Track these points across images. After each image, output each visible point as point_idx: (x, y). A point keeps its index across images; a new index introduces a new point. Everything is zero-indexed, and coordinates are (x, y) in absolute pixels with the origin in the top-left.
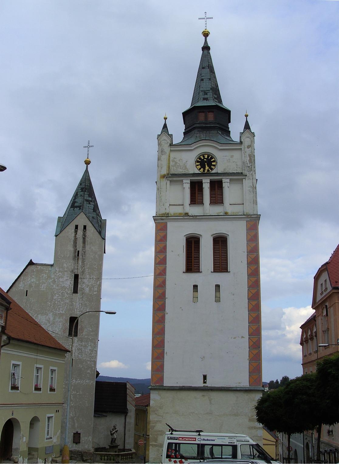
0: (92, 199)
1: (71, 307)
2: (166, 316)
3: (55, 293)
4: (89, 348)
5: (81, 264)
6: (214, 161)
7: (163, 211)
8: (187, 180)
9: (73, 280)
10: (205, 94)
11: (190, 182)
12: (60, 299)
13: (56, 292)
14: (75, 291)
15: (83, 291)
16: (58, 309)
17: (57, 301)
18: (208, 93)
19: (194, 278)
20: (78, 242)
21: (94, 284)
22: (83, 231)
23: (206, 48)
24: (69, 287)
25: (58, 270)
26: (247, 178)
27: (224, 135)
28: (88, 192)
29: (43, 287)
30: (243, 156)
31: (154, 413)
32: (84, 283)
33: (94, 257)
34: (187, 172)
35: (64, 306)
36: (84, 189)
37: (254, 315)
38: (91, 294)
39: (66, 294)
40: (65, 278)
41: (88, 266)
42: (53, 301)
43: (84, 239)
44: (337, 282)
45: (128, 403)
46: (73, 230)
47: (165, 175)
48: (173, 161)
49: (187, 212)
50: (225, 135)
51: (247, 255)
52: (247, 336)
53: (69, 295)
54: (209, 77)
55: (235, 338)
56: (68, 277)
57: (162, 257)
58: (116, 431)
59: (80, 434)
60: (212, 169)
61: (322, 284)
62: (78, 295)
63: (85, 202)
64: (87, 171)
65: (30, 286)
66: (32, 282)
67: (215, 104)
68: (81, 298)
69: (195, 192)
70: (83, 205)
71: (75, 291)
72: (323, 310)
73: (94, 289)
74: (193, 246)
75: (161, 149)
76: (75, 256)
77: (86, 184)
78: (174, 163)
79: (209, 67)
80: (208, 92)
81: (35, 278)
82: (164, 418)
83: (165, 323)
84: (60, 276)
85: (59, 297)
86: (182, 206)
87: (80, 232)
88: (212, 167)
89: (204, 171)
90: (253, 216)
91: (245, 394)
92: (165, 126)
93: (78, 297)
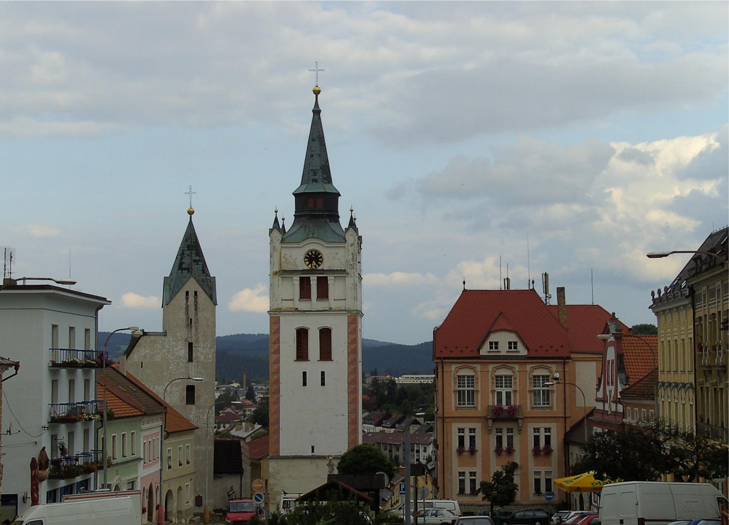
6: (321, 261)
12: (176, 368)
14: (190, 359)
19: (303, 366)
23: (317, 112)
26: (349, 276)
28: (195, 250)
29: (158, 358)
30: (347, 254)
32: (198, 351)
34: (296, 269)
43: (196, 306)
46: (184, 297)
48: (284, 257)
49: (297, 307)
54: (319, 153)
55: (337, 416)
58: (233, 493)
59: (201, 497)
60: (319, 265)
62: (194, 363)
63: (194, 263)
64: (191, 223)
65: (145, 357)
76: (188, 324)
78: (285, 260)
79: (319, 138)
80: (317, 171)
86: (292, 301)
88: (319, 263)
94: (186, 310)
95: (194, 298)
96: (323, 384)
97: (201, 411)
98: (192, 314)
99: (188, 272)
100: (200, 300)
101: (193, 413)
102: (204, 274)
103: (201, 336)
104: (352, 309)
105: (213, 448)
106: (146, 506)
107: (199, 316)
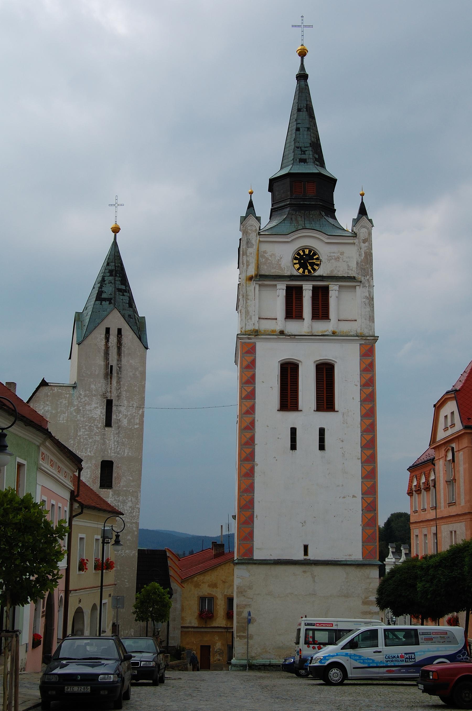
0: (126, 287)
1: (103, 447)
2: (256, 468)
3: (80, 427)
4: (129, 504)
5: (115, 385)
7: (250, 327)
8: (282, 285)
9: (105, 408)
10: (303, 153)
11: (285, 288)
12: (87, 434)
13: (81, 426)
14: (108, 423)
15: (120, 424)
16: (84, 450)
17: (83, 438)
18: (306, 151)
20: (110, 353)
21: (134, 414)
22: (118, 336)
24: (100, 418)
25: (83, 394)
27: (329, 217)
28: (119, 277)
31: (242, 595)
32: (120, 412)
33: (133, 374)
35: (94, 446)
36: (114, 272)
37: (369, 468)
38: (131, 428)
39: (96, 428)
40: (94, 405)
41: (126, 388)
42: (77, 439)
44: (470, 419)
45: (171, 579)
46: (103, 336)
47: (253, 276)
50: (329, 216)
51: (360, 389)
52: (359, 496)
53: (99, 430)
55: (344, 497)
56: (97, 404)
57: (249, 390)
60: (314, 270)
61: (446, 417)
62: (113, 429)
64: (115, 244)
66: (47, 412)
67: (317, 171)
68: (116, 434)
69: (292, 301)
70: (115, 297)
71: (108, 423)
72: (446, 452)
73: (134, 421)
74: (289, 375)
75: (247, 239)
77: (116, 265)
79: (307, 108)
80: (306, 149)
81: (50, 405)
82: (254, 601)
83: (254, 477)
84: (86, 401)
85: (86, 433)
86: (275, 321)
87: (113, 339)
89: (304, 272)
90: (368, 338)
91: (358, 570)
92: (251, 205)
93: (112, 432)
94: (105, 354)
95: (116, 337)
96: (322, 447)
97: (121, 498)
99: (110, 303)
100: (125, 340)
102: (131, 309)
103: (126, 391)
104: (367, 335)
105: (137, 554)
106: (41, 632)
107: (123, 363)
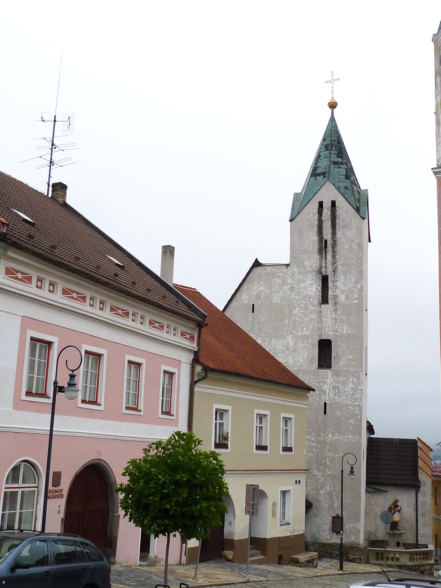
12: (303, 313)
14: (325, 300)
29: (276, 299)
64: (332, 119)
65: (258, 297)
98: (327, 234)
100: (339, 212)
101: (329, 381)
